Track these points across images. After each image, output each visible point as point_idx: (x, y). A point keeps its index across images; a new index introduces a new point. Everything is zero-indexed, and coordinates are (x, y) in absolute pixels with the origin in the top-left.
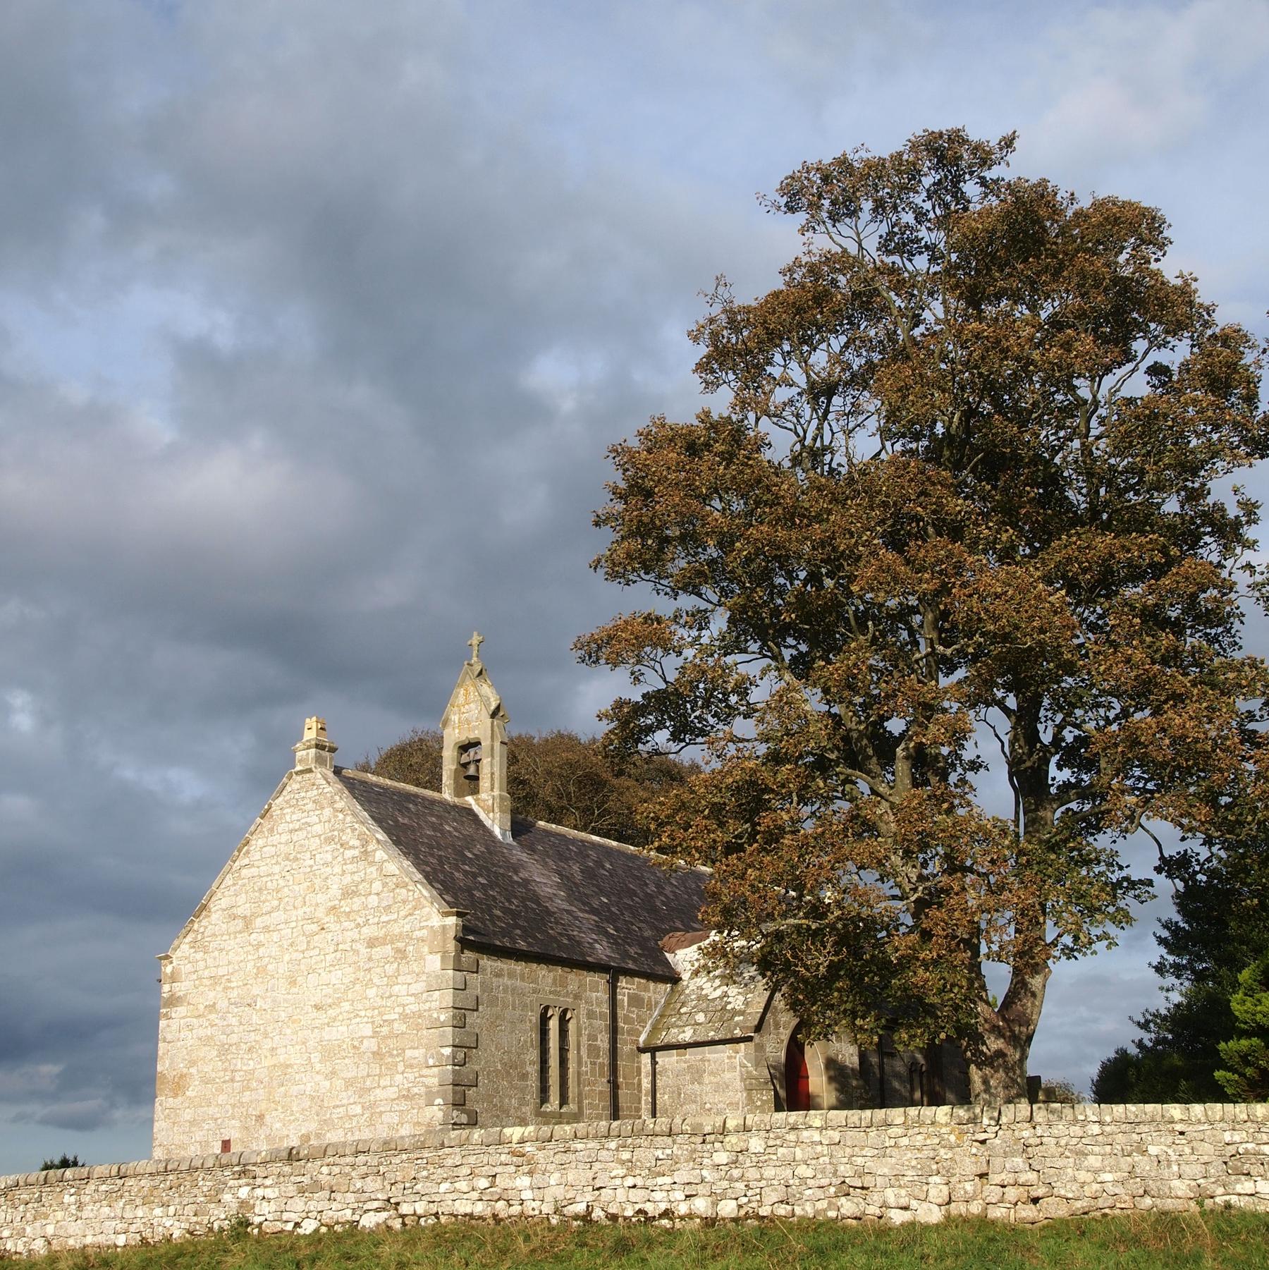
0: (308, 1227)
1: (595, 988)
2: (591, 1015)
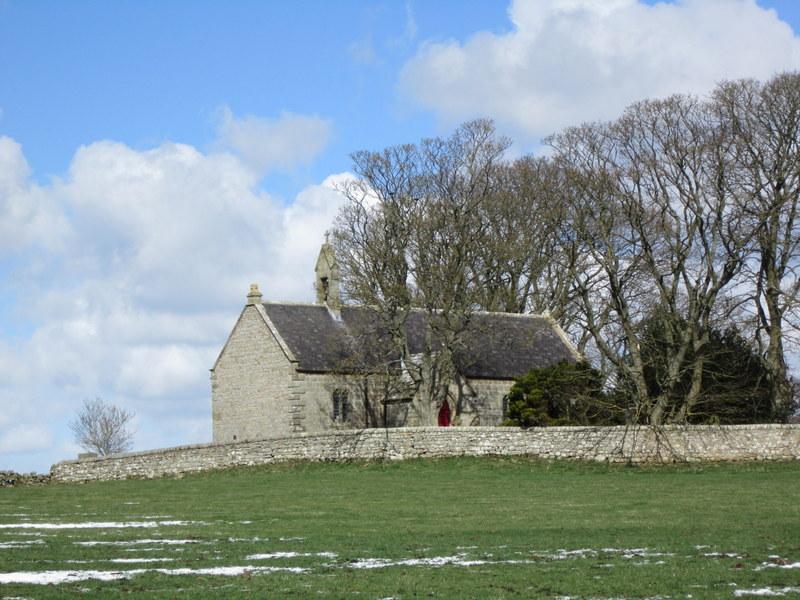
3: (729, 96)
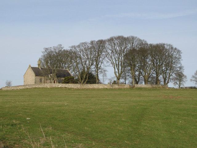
3: (92, 43)
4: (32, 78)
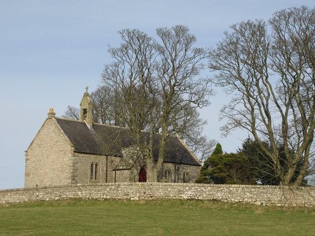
0: (48, 199)
1: (103, 159)
2: (102, 164)
4: (59, 161)
